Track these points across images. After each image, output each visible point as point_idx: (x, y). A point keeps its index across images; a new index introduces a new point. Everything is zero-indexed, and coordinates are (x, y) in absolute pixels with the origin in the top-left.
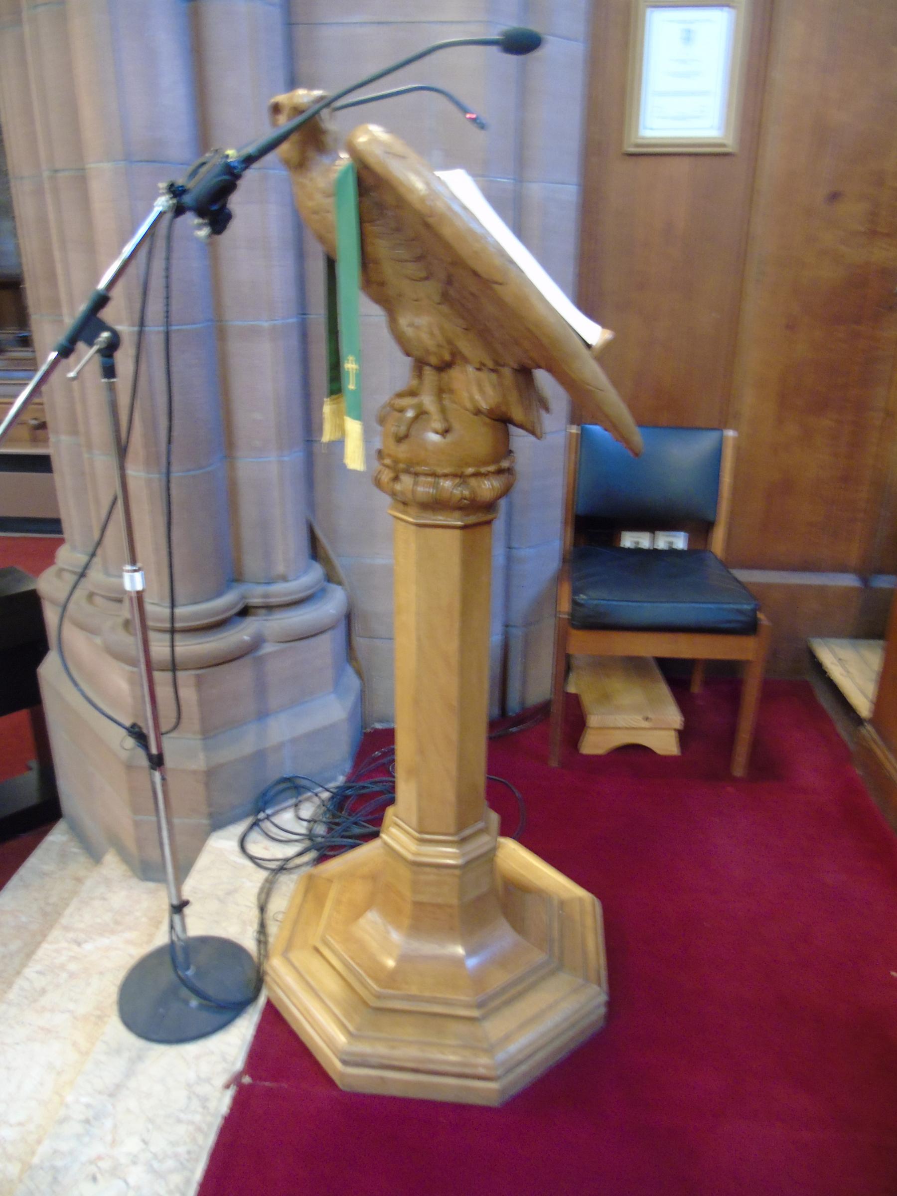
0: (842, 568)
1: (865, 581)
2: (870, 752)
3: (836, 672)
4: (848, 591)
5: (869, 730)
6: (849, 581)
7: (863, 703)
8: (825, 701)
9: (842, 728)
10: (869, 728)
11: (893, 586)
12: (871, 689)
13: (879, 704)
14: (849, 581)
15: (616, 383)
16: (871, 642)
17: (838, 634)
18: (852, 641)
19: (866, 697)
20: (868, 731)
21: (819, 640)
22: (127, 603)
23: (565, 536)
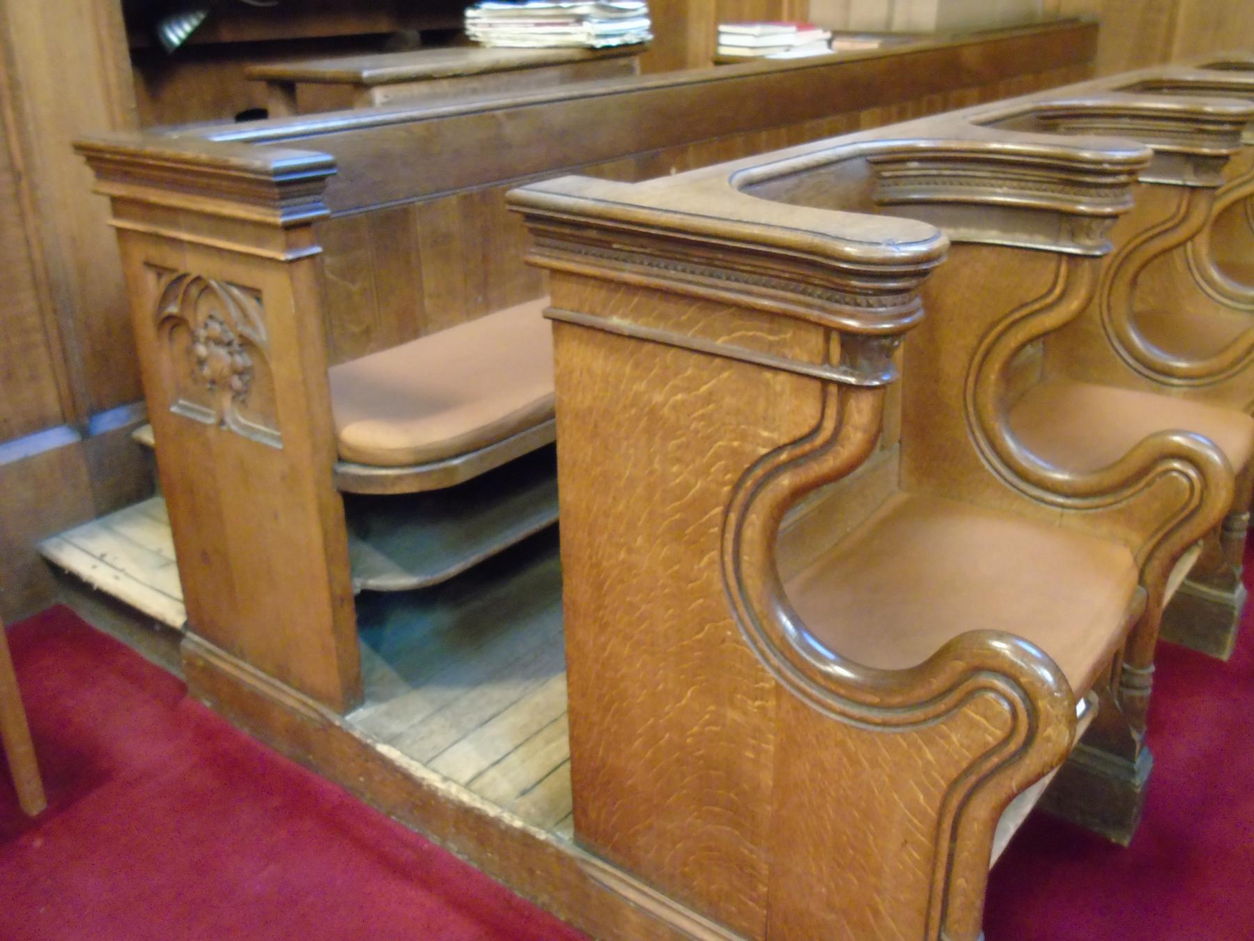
0: (39, 424)
1: (85, 432)
2: (210, 672)
3: (102, 577)
4: (63, 452)
5: (193, 640)
6: (57, 439)
7: (172, 612)
8: (103, 623)
9: (147, 650)
10: (190, 635)
11: (1062, 725)
12: (171, 581)
13: (191, 600)
14: (57, 439)
15: (827, 717)
16: (129, 510)
17: (75, 519)
18: (101, 521)
19: (177, 600)
20: (194, 642)
21: (55, 540)
22: (202, 340)
23: (864, 292)
